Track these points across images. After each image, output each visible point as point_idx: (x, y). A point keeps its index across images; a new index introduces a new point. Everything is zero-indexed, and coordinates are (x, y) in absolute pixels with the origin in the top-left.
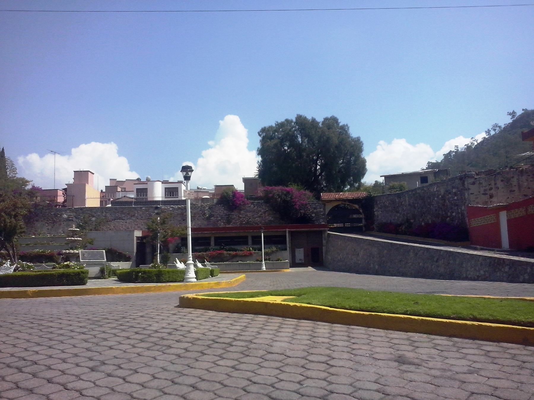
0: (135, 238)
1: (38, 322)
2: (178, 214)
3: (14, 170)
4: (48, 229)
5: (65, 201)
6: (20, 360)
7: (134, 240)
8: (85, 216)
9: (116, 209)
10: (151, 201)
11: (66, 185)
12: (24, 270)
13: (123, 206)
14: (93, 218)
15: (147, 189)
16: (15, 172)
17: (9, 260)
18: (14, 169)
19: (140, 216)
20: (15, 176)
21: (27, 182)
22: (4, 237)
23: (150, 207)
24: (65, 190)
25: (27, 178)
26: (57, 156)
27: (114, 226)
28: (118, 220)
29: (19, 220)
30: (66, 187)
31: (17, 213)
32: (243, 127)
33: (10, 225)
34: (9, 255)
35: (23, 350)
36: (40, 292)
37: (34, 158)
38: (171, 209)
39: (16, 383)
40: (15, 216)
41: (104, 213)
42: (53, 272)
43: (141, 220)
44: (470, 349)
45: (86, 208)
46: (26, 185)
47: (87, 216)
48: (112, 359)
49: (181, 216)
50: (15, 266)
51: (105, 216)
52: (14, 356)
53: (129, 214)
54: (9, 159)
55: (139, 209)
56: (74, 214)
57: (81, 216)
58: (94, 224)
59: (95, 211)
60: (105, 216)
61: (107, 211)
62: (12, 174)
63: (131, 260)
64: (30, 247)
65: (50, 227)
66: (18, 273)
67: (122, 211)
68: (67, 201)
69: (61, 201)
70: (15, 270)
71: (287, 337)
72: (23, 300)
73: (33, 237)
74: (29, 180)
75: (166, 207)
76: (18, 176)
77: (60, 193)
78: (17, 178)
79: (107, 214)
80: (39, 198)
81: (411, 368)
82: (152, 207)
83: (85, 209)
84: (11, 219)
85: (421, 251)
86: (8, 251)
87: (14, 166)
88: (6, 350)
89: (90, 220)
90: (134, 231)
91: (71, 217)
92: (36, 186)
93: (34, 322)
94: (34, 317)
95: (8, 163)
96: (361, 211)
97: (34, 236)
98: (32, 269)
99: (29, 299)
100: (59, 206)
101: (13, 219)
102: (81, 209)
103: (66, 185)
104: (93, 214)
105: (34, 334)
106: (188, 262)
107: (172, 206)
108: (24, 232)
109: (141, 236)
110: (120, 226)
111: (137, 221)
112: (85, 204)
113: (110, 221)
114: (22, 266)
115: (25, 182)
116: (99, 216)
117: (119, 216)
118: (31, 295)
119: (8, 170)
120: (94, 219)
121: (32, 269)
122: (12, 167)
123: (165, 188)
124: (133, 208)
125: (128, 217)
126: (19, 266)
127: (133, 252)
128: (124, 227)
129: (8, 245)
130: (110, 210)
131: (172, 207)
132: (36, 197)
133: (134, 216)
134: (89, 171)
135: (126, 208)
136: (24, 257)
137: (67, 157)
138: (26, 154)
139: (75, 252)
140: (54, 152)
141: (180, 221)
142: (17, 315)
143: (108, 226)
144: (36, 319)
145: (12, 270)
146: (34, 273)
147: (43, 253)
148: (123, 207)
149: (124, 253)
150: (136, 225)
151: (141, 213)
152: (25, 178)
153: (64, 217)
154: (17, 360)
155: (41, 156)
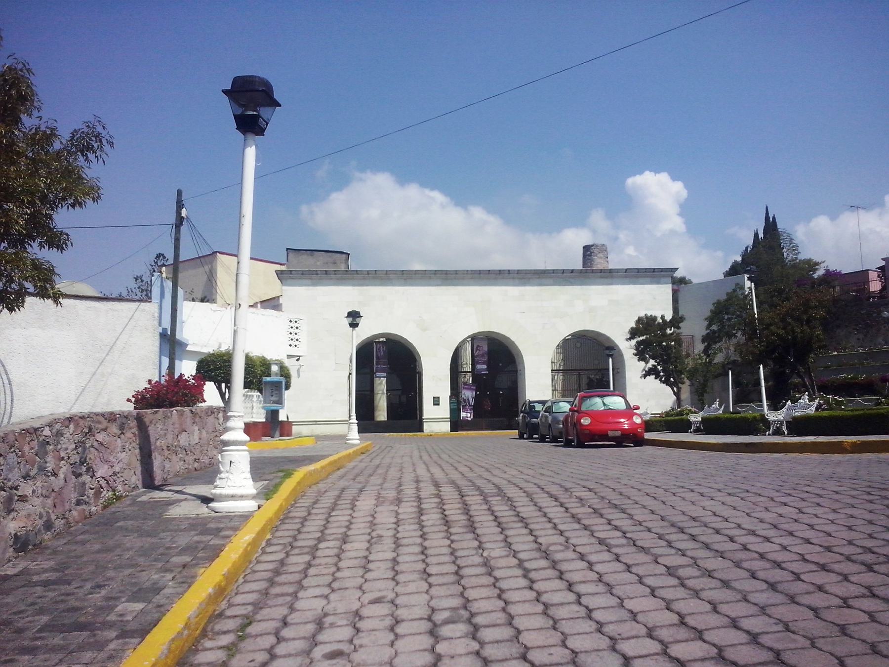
1: (878, 493)
3: (795, 249)
4: (858, 339)
5: (884, 288)
6: (865, 552)
11: (883, 259)
12: (831, 409)
16: (796, 252)
17: (807, 393)
18: (793, 247)
20: (796, 258)
21: (817, 264)
22: (794, 357)
24: (882, 268)
25: (816, 258)
26: (862, 212)
29: (815, 327)
30: (883, 263)
31: (811, 316)
32: (669, 177)
33: (801, 337)
34: (805, 386)
35: (866, 536)
36: (864, 443)
37: (822, 222)
39: (869, 588)
40: (808, 321)
42: (882, 411)
44: (559, 592)
46: (815, 271)
48: (832, 563)
50: (817, 401)
52: (854, 545)
54: (785, 233)
62: (791, 255)
65: (861, 336)
66: (825, 413)
69: (876, 290)
70: (817, 409)
71: (524, 543)
72: (837, 457)
74: (820, 261)
76: (802, 257)
77: (873, 275)
78: (800, 260)
80: (838, 288)
81: (101, 582)
84: (802, 326)
85: (68, 443)
86: (803, 380)
87: (794, 242)
88: (838, 533)
92: (831, 268)
93: (872, 493)
94: (869, 484)
95: (784, 239)
97: (835, 353)
98: (843, 407)
99: (848, 456)
100: (874, 297)
101: (805, 327)
103: (883, 259)
105: (877, 512)
106: (226, 437)
108: (825, 346)
114: (827, 402)
115: (812, 265)
118: (849, 449)
119: (785, 250)
121: (843, 407)
122: (790, 244)
126: (821, 402)
129: (801, 369)
132: (834, 287)
136: (825, 388)
137: (877, 211)
138: (808, 220)
140: (854, 207)
142: (840, 480)
144: (873, 487)
145: (814, 409)
146: (850, 413)
147: (854, 381)
152: (812, 258)
153: (884, 316)
154: (859, 550)
155: (833, 217)
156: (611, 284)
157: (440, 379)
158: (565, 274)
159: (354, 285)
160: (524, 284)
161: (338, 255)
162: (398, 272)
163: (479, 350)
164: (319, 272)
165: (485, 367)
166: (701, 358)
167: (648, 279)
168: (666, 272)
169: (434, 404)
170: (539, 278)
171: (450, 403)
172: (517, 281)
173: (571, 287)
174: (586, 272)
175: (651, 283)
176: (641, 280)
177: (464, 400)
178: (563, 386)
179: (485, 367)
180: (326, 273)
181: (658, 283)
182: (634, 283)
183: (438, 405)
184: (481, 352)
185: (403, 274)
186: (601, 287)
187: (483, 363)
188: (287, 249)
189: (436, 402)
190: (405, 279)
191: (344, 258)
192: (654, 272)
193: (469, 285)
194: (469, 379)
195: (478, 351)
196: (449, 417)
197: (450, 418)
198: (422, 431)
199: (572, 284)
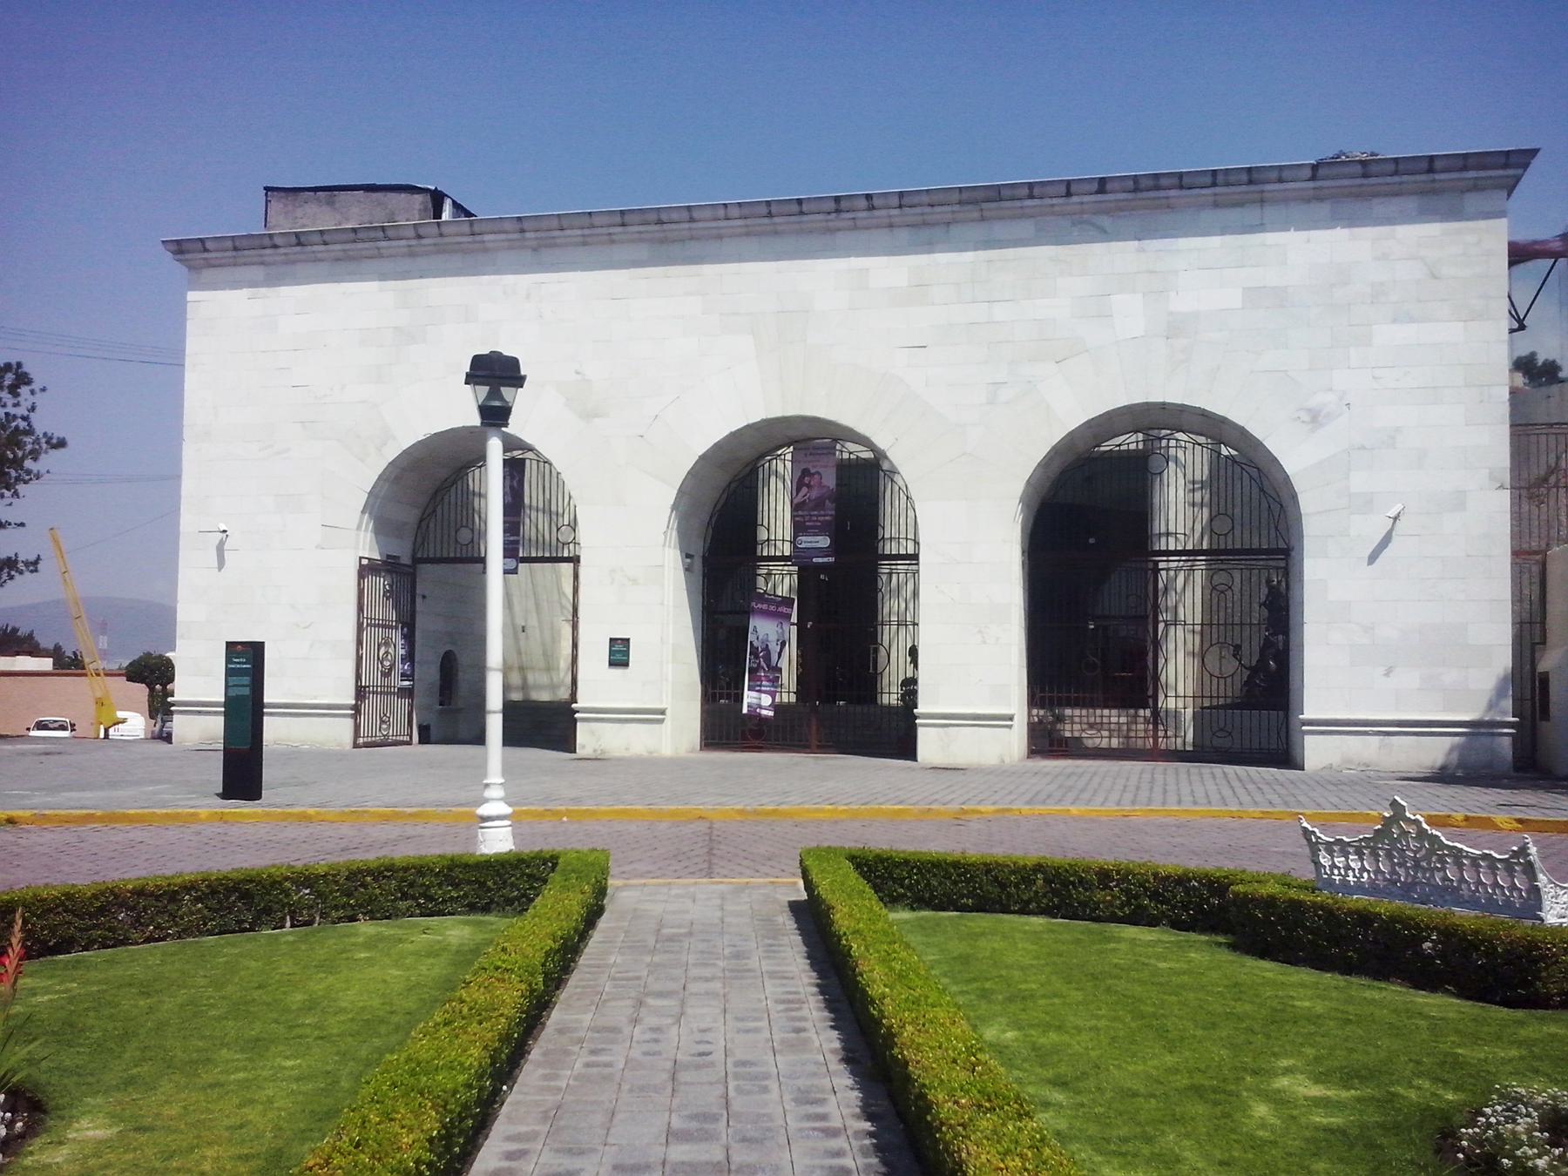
156: (1260, 227)
157: (634, 581)
158: (1075, 199)
159: (383, 277)
160: (929, 247)
161: (403, 197)
162: (507, 226)
163: (808, 486)
164: (278, 241)
165: (824, 542)
166: (364, 209)
167: (1411, 203)
168: (1484, 168)
169: (612, 664)
170: (983, 219)
171: (229, 673)
172: (903, 235)
173: (1099, 248)
174: (1157, 188)
175: (1424, 215)
176: (1379, 207)
177: (755, 652)
178: (1208, 608)
179: (824, 542)
180: (299, 240)
181: (1454, 214)
182: (1352, 222)
183: (625, 664)
184: (814, 494)
185: (522, 231)
186: (1215, 241)
187: (821, 530)
188: (265, 188)
189: (618, 657)
190: (535, 250)
191: (417, 206)
192: (1431, 170)
193: (740, 258)
194: (783, 582)
195: (805, 490)
196: (265, 718)
197: (575, 721)
198: (575, 752)
199: (1105, 235)
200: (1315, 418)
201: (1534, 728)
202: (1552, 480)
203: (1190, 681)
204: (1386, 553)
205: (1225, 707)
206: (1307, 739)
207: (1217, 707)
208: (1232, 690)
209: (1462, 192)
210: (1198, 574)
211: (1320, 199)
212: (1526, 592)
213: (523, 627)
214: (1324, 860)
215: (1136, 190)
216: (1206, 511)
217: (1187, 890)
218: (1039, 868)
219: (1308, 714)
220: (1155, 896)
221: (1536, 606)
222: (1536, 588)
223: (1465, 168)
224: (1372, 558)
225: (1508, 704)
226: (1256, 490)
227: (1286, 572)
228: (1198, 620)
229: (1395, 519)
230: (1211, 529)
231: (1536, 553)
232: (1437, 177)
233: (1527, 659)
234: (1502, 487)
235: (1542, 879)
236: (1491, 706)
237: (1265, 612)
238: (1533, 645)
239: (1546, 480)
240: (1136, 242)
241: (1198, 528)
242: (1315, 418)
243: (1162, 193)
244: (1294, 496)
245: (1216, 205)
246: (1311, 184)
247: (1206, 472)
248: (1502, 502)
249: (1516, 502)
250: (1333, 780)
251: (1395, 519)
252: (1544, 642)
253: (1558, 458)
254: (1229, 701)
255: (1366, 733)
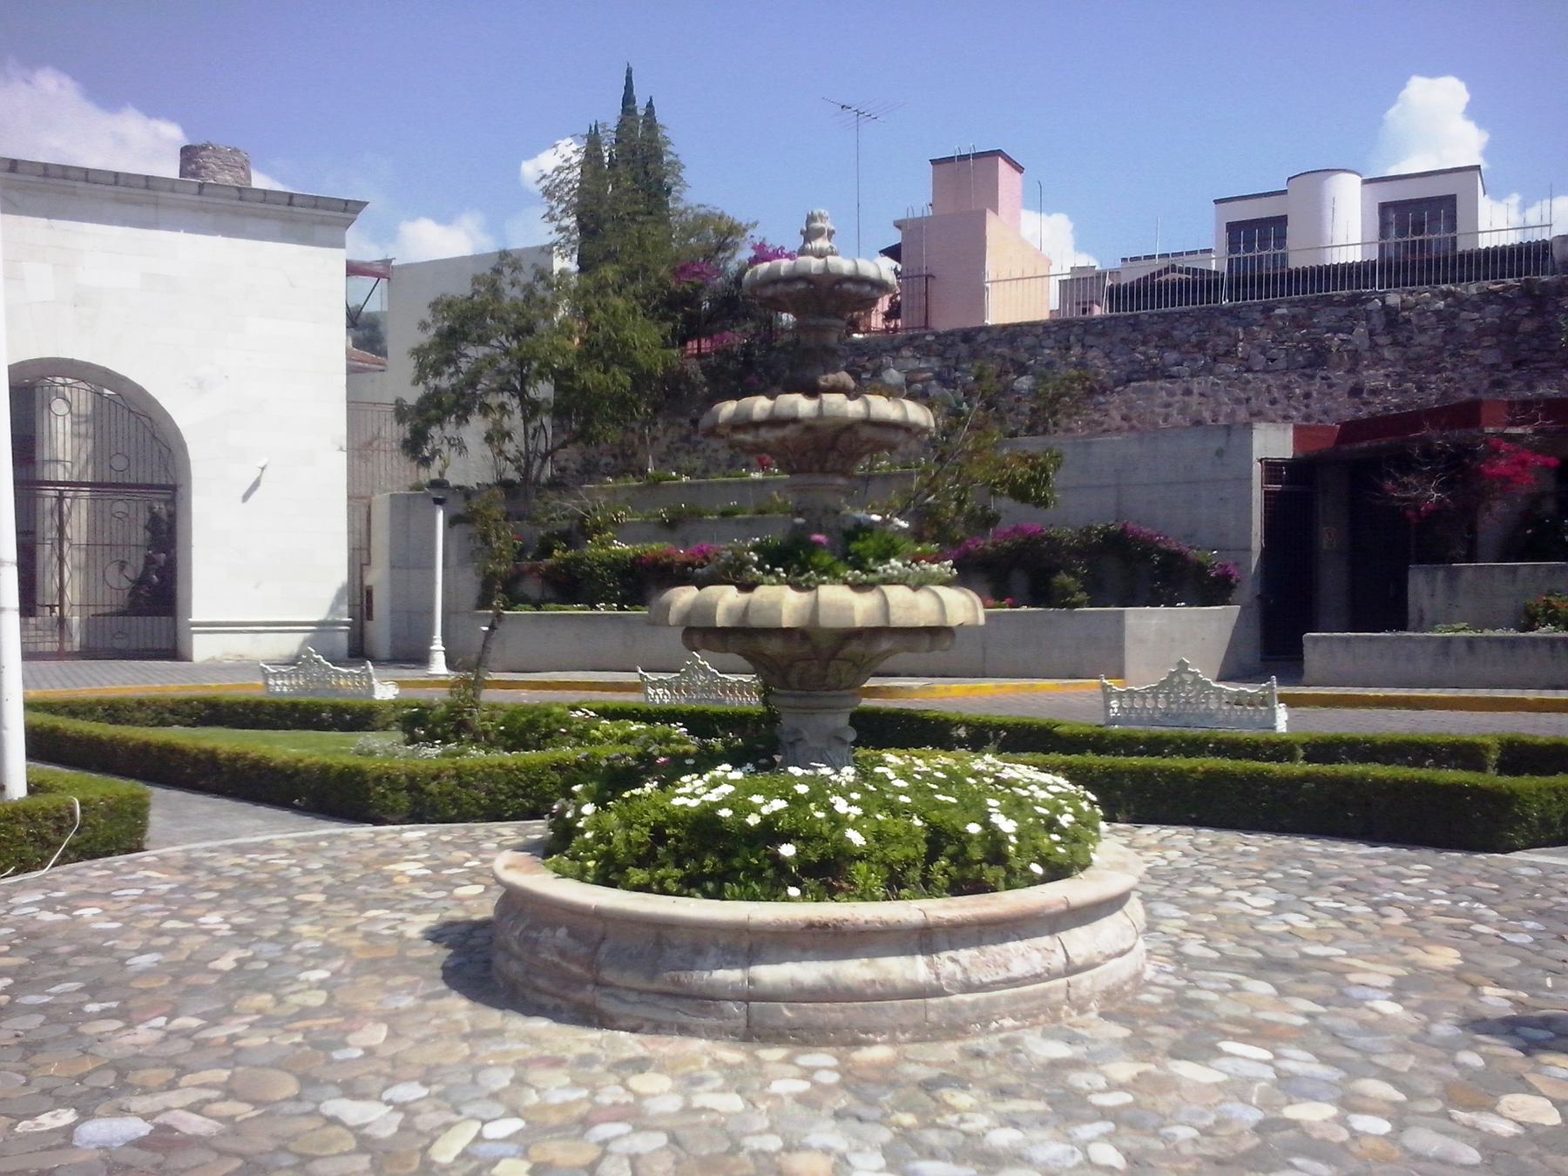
0: (1257, 469)
2: (1481, 332)
7: (1250, 478)
8: (982, 368)
9: (1135, 324)
10: (1335, 267)
11: (898, 225)
13: (1170, 309)
14: (1023, 379)
15: (1281, 222)
19: (1262, 352)
23: (1316, 301)
27: (1124, 410)
28: (1148, 383)
38: (1441, 304)
41: (1076, 350)
43: (1267, 377)
45: (988, 329)
47: (992, 367)
49: (1504, 338)
51: (1081, 364)
53: (1201, 346)
55: (1257, 316)
56: (935, 363)
57: (968, 372)
58: (1026, 407)
59: (1029, 341)
60: (1081, 364)
61: (1089, 340)
63: (1235, 595)
64: (738, 522)
67: (1165, 335)
68: (903, 313)
73: (755, 482)
75: (1411, 293)
79: (1092, 353)
82: (1329, 301)
83: (982, 337)
89: (1008, 389)
90: (1248, 427)
91: (922, 381)
96: (1345, 447)
97: (757, 476)
102: (968, 336)
103: (898, 225)
104: (1023, 356)
107: (1444, 287)
109: (1289, 456)
110: (1157, 410)
111: (1248, 382)
112: (977, 296)
113: (1103, 390)
116: (1050, 365)
117: (1149, 358)
120: (1024, 383)
123: (1384, 208)
124: (1225, 312)
125: (1195, 360)
127: (1248, 549)
128: (1176, 418)
130: (1102, 334)
131: (1449, 294)
133: (1227, 353)
134: (998, 153)
135: (1184, 314)
139: (828, 620)
141: (1494, 366)
143: (1096, 416)
148: (1171, 313)
149: (1193, 554)
150: (1238, 401)
151: (1265, 336)
174: (65, 178)
178: (93, 529)
200: (200, 385)
201: (362, 627)
202: (375, 444)
203: (77, 591)
204: (255, 495)
205: (111, 614)
206: (196, 638)
207: (104, 615)
208: (120, 600)
209: (314, 223)
210: (83, 502)
211: (206, 210)
212: (357, 526)
213: (1446, 654)
214: (271, 682)
215: (46, 175)
216: (90, 442)
217: (192, 708)
218: (99, 702)
219: (194, 619)
220: (172, 712)
221: (364, 535)
222: (364, 522)
223: (316, 207)
224: (246, 497)
225: (345, 608)
226: (148, 435)
227: (172, 501)
228: (84, 541)
229: (263, 469)
230: (96, 457)
231: (363, 498)
232: (295, 209)
233: (358, 575)
234: (341, 449)
235: (375, 681)
236: (333, 609)
237: (148, 534)
238: (362, 565)
239: (370, 444)
240: (45, 220)
241: (83, 456)
242: (200, 385)
243: (69, 183)
244: (183, 446)
245: (118, 200)
246: (198, 198)
247: (90, 408)
248: (342, 459)
249: (350, 459)
250: (214, 667)
251: (263, 469)
252: (369, 564)
253: (379, 429)
254: (114, 609)
255: (241, 632)
